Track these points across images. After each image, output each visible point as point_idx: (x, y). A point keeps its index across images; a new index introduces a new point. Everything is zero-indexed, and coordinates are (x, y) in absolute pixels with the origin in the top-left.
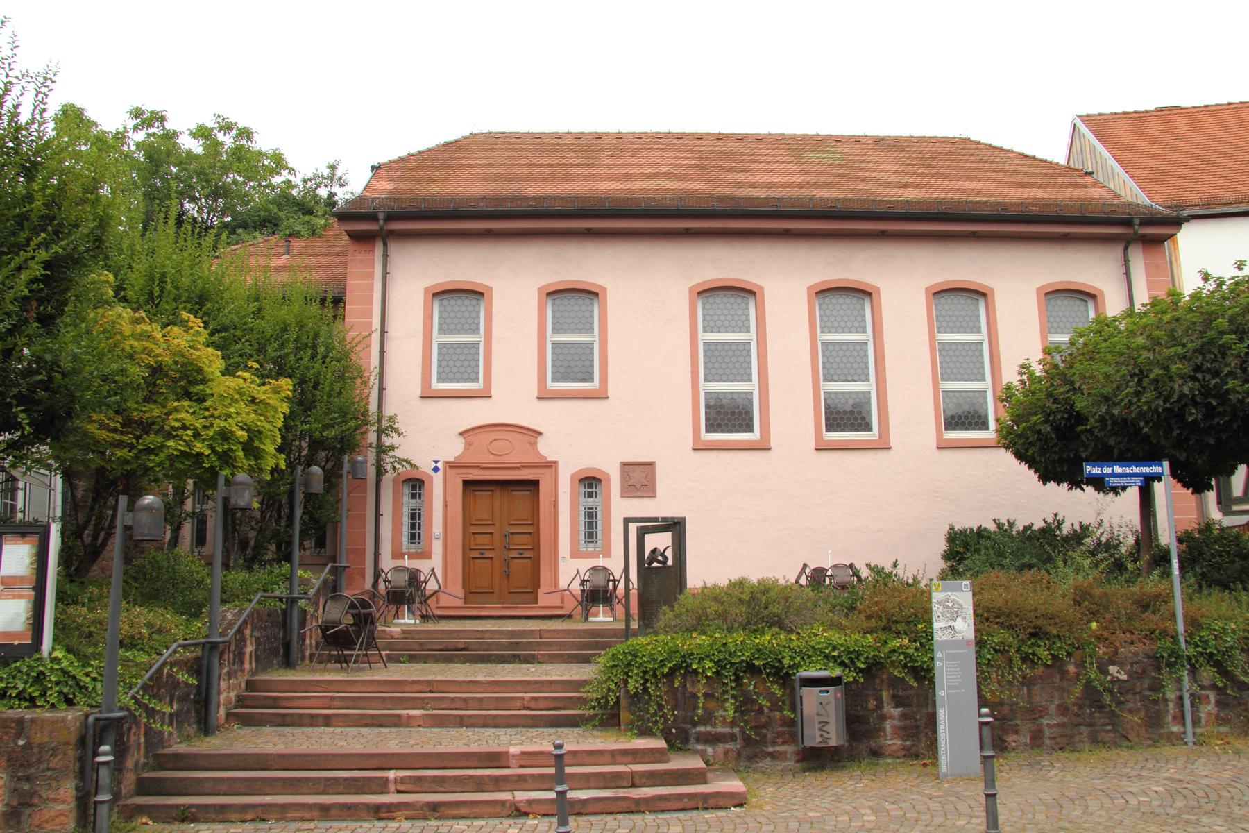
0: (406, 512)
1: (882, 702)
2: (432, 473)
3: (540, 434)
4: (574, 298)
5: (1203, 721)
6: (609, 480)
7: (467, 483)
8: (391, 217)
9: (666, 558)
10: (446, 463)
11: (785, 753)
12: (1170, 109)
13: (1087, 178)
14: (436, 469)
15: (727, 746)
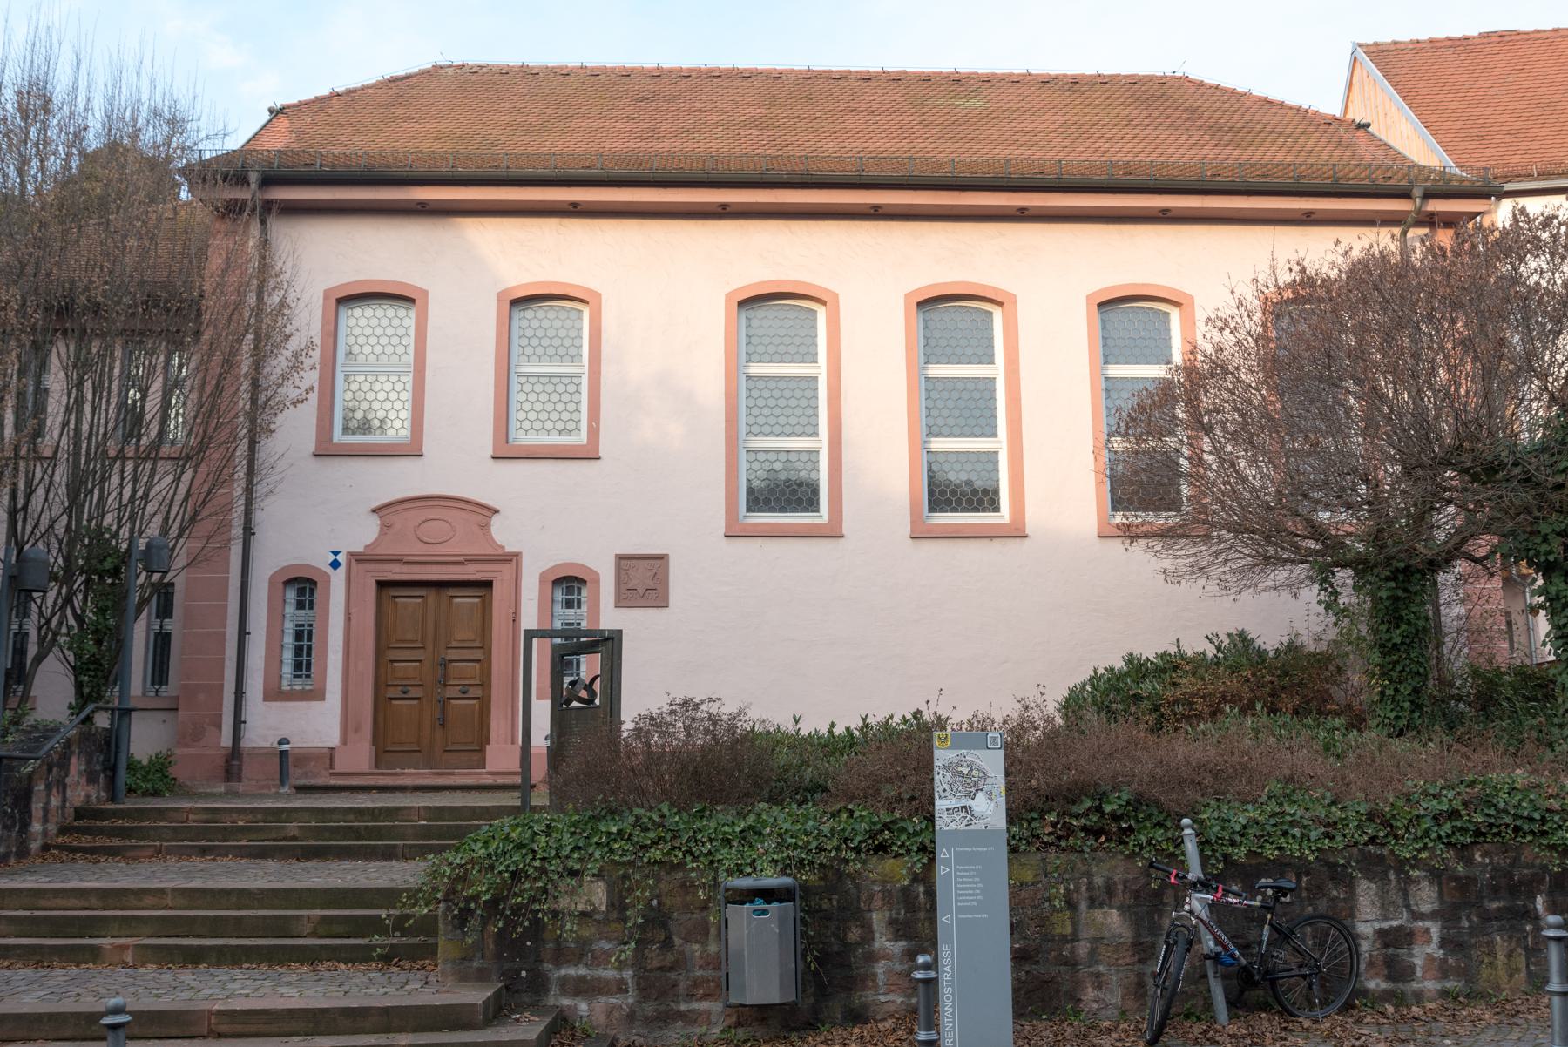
0: (289, 627)
1: (872, 932)
2: (329, 570)
3: (496, 511)
4: (948, 314)
5: (1419, 973)
6: (597, 581)
7: (381, 585)
8: (268, 181)
9: (593, 694)
10: (351, 554)
11: (708, 1013)
12: (1501, 35)
13: (1360, 133)
14: (335, 565)
15: (613, 1001)
